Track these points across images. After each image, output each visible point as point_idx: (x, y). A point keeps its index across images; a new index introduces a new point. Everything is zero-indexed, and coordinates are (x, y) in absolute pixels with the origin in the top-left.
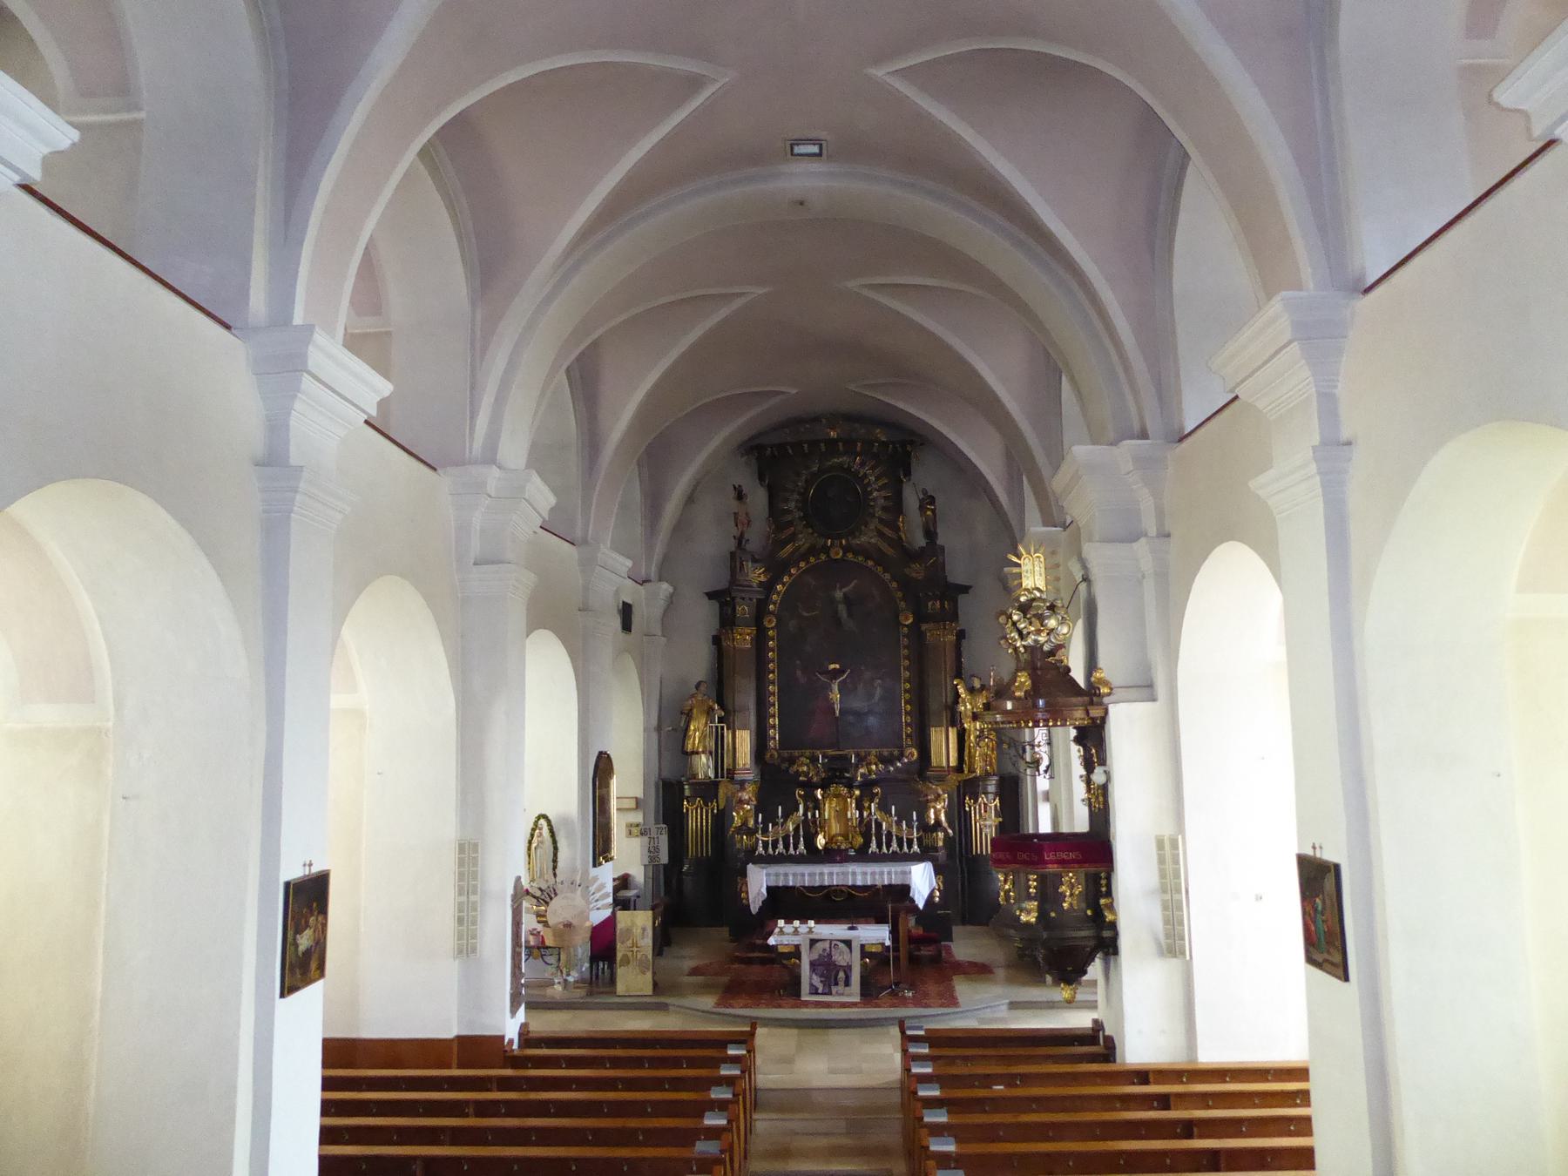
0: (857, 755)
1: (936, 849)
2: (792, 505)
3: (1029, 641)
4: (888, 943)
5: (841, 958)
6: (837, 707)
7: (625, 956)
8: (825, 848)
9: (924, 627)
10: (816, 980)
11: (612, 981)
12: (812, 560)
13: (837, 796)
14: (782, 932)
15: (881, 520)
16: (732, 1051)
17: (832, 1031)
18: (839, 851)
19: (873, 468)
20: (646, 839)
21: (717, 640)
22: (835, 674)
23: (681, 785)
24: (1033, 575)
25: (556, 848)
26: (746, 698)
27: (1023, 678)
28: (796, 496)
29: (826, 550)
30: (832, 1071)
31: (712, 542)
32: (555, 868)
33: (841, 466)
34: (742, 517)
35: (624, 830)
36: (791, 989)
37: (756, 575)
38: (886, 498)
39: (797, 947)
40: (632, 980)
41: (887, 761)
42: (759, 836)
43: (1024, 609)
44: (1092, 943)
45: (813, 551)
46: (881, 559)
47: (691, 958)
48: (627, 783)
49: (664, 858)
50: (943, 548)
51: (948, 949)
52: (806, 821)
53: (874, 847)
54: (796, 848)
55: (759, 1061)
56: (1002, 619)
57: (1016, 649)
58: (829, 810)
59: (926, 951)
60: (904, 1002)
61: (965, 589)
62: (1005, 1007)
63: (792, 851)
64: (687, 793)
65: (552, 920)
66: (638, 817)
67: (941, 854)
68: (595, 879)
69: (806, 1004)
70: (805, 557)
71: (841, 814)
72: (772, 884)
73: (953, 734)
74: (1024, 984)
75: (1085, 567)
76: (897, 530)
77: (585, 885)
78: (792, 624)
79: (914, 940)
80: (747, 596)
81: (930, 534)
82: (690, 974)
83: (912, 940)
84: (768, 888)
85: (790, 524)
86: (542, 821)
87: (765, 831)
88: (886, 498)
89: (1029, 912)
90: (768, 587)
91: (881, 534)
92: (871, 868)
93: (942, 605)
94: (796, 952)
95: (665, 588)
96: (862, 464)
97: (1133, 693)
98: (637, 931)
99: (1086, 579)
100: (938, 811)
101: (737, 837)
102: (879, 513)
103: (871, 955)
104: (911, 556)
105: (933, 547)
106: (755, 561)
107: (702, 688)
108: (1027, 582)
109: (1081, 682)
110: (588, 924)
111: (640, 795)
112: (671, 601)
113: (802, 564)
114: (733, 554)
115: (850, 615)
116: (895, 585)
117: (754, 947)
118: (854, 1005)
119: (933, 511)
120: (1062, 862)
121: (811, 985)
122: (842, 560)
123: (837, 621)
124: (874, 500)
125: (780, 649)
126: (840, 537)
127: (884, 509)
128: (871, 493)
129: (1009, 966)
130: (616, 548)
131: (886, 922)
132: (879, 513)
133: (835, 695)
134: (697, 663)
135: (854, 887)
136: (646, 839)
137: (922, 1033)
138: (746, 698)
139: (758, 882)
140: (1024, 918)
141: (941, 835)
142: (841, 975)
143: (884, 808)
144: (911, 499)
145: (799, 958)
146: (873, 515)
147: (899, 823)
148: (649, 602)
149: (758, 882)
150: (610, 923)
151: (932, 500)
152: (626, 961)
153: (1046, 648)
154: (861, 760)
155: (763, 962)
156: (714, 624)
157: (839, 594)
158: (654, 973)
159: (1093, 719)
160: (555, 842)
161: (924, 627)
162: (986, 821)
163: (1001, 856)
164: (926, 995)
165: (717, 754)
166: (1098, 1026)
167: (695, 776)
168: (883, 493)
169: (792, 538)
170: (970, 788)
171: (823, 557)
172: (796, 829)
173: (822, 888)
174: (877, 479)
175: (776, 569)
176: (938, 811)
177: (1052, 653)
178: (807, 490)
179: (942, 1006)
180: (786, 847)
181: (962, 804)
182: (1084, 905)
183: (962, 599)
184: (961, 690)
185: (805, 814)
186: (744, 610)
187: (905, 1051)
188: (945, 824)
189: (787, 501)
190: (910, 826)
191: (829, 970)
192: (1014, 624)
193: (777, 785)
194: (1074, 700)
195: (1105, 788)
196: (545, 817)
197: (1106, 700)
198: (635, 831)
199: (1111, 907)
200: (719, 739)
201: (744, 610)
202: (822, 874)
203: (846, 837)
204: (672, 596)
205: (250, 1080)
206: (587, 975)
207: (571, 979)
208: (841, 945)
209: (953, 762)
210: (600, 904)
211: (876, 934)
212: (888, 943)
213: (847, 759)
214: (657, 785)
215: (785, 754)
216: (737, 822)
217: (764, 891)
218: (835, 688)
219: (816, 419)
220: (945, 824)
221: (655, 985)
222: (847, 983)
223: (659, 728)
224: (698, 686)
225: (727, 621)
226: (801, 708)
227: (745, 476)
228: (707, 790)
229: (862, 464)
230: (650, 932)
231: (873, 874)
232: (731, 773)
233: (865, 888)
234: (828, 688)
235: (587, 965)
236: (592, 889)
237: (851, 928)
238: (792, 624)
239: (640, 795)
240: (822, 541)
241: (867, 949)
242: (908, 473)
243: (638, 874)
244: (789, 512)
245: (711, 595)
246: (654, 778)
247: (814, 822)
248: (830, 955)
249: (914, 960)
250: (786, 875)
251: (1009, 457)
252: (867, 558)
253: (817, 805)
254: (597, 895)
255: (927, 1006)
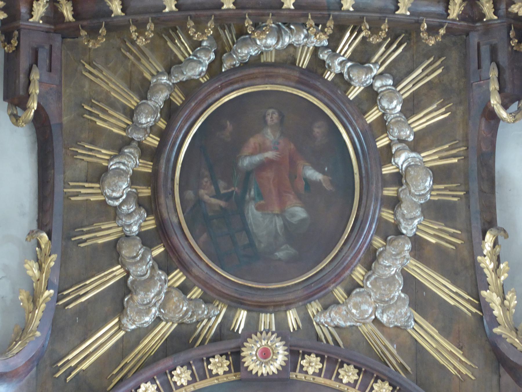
2: (119, 190)
19: (397, 72)
33: (287, 60)
38: (440, 175)
76: (473, 281)
85: (112, 252)
88: (440, 175)
91: (418, 296)
96: (361, 58)
102: (413, 223)
122: (281, 379)
126: (279, 307)
127: (435, 210)
128: (387, 155)
132: (413, 223)
168: (431, 157)
174: (411, 107)
205: (201, 387)
229: (361, 58)
240: (212, 317)
244: (108, 212)
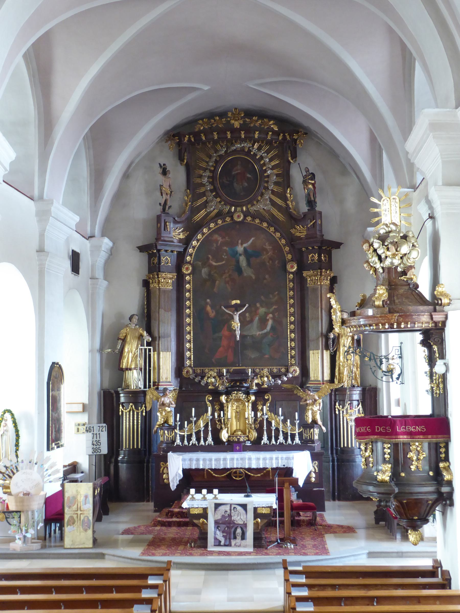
0: (253, 371)
1: (313, 442)
2: (205, 180)
3: (387, 263)
4: (275, 506)
5: (239, 517)
6: (238, 333)
7: (72, 517)
8: (228, 441)
9: (305, 274)
10: (220, 536)
11: (62, 538)
12: (220, 222)
13: (238, 400)
14: (193, 499)
15: (273, 192)
16: (151, 581)
17: (230, 572)
18: (239, 442)
19: (268, 152)
20: (90, 435)
21: (146, 284)
22: (237, 308)
23: (118, 394)
24: (389, 211)
25: (18, 436)
26: (167, 326)
27: (382, 292)
28: (208, 173)
29: (231, 214)
30: (230, 600)
31: (141, 209)
32: (17, 450)
34: (166, 189)
35: (74, 429)
36: (201, 541)
37: (176, 233)
38: (277, 175)
39: (205, 509)
40: (77, 535)
41: (276, 376)
42: (177, 431)
43: (383, 239)
44: (434, 497)
45: (220, 215)
46: (273, 222)
47: (126, 522)
48: (78, 391)
49: (104, 450)
50: (320, 213)
51: (322, 516)
52: (213, 420)
53: (265, 439)
54: (205, 440)
55: (173, 593)
56: (365, 247)
57: (376, 270)
58: (231, 411)
59: (304, 516)
60: (287, 552)
61: (338, 245)
62: (365, 556)
63: (202, 443)
64: (122, 400)
65: (13, 490)
66: (84, 418)
67: (317, 446)
68: (48, 459)
69: (212, 553)
70: (214, 219)
71: (240, 415)
72: (187, 467)
73: (327, 355)
74: (381, 540)
75: (431, 208)
76: (285, 199)
77: (39, 464)
78: (204, 271)
79: (295, 509)
80: (170, 249)
81: (311, 203)
82: (123, 533)
83: (294, 508)
84: (184, 471)
85: (204, 194)
86: (8, 415)
87: (182, 427)
88: (277, 175)
89: (384, 473)
90: (187, 242)
91: (273, 203)
92: (262, 455)
93: (320, 256)
94: (204, 514)
95: (107, 243)
96: (259, 149)
97: (446, 485)
98: (81, 499)
99: (431, 217)
100: (315, 411)
101: (160, 432)
102: (271, 187)
103: (262, 516)
104: (294, 219)
105: (313, 211)
106: (175, 222)
107: (135, 320)
108: (385, 219)
109: (427, 296)
110: (42, 493)
111: (86, 401)
112: (112, 253)
113: (212, 225)
114: (159, 218)
115: (249, 264)
116: (283, 241)
117: (172, 515)
118: (249, 553)
119: (313, 185)
120: (411, 434)
121: (216, 539)
123: (239, 270)
124: (268, 176)
125: (195, 291)
126: (242, 206)
127: (276, 183)
128: (265, 171)
129: (368, 527)
130: (65, 204)
131: (273, 491)
132: (271, 187)
133: (236, 324)
134: (131, 300)
135: (249, 469)
136: (90, 435)
137: (300, 568)
138: (167, 326)
139: (176, 466)
140: (380, 477)
141: (317, 431)
142: (239, 531)
143: (273, 410)
144: (297, 175)
145: (206, 519)
146: (267, 188)
147: (284, 421)
148: (95, 254)
149: (176, 466)
150: (60, 495)
151: (313, 176)
152: (72, 522)
153: (399, 269)
154: (256, 374)
155: (179, 524)
156: (144, 273)
157: (240, 249)
158: (94, 532)
159: (436, 323)
160: (17, 431)
161: (305, 274)
162: (351, 413)
163: (363, 430)
164: (304, 547)
165: (147, 370)
166: (438, 565)
167: (128, 386)
168: (275, 171)
169: (205, 205)
170: (339, 395)
171: (228, 219)
172: (206, 426)
173: (225, 470)
175: (192, 229)
176: (315, 411)
177: (404, 273)
178: (216, 168)
179: (317, 554)
180: (198, 439)
181: (332, 408)
182: (427, 468)
183: (335, 252)
184: (333, 302)
185: (213, 414)
186: (168, 260)
187: (287, 580)
188: (320, 422)
189: (201, 176)
190: (293, 424)
191: (230, 529)
192: (375, 250)
193: (191, 395)
194: (421, 308)
195: (444, 377)
196: (9, 411)
197: (446, 308)
198: (82, 428)
199: (448, 469)
200: (147, 359)
201: (168, 260)
202: (225, 459)
203: (244, 433)
204: (112, 248)
206: (42, 534)
207: (29, 535)
208: (239, 508)
209: (327, 377)
210: (52, 478)
211: (266, 501)
212: (275, 506)
213: (244, 372)
214: (99, 394)
215: (198, 370)
216: (161, 420)
217: (181, 472)
218: (237, 318)
219: (223, 115)
220: (320, 422)
221: (95, 541)
222: (243, 537)
223: (101, 350)
224: (131, 319)
225: (154, 268)
226: (210, 328)
227: (168, 157)
228: (137, 397)
230: (91, 499)
231: (264, 459)
232: (156, 385)
233: (258, 470)
234: (232, 318)
235: (41, 524)
236: (46, 466)
237: (247, 496)
238: (204, 271)
239: (86, 401)
241: (259, 511)
242: (294, 156)
243: (84, 463)
245: (142, 249)
246: (97, 388)
247: (220, 421)
248: (230, 516)
249: (295, 524)
250: (198, 460)
251: (373, 140)
252: (262, 221)
253: (222, 407)
254: (50, 472)
255: (305, 554)
